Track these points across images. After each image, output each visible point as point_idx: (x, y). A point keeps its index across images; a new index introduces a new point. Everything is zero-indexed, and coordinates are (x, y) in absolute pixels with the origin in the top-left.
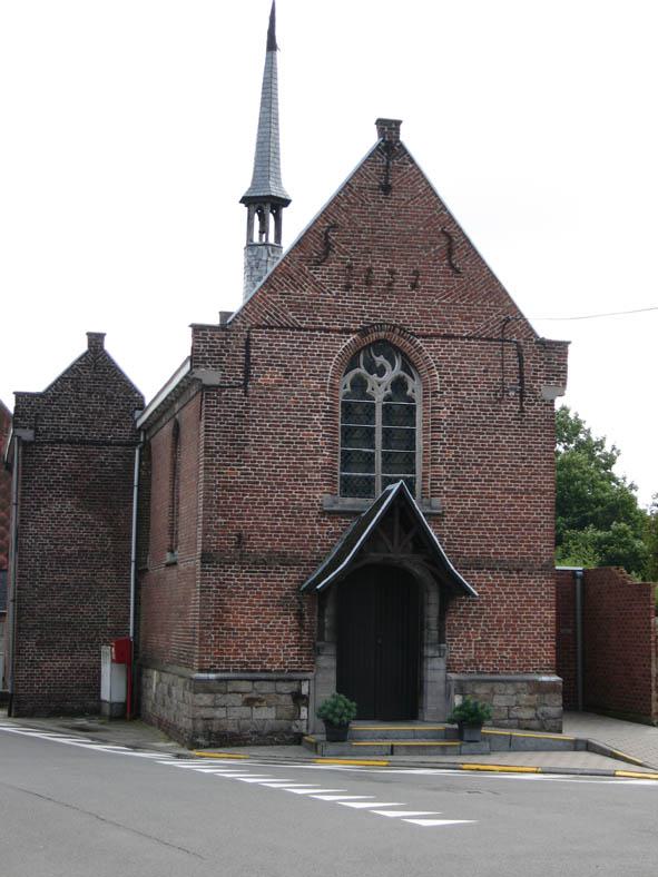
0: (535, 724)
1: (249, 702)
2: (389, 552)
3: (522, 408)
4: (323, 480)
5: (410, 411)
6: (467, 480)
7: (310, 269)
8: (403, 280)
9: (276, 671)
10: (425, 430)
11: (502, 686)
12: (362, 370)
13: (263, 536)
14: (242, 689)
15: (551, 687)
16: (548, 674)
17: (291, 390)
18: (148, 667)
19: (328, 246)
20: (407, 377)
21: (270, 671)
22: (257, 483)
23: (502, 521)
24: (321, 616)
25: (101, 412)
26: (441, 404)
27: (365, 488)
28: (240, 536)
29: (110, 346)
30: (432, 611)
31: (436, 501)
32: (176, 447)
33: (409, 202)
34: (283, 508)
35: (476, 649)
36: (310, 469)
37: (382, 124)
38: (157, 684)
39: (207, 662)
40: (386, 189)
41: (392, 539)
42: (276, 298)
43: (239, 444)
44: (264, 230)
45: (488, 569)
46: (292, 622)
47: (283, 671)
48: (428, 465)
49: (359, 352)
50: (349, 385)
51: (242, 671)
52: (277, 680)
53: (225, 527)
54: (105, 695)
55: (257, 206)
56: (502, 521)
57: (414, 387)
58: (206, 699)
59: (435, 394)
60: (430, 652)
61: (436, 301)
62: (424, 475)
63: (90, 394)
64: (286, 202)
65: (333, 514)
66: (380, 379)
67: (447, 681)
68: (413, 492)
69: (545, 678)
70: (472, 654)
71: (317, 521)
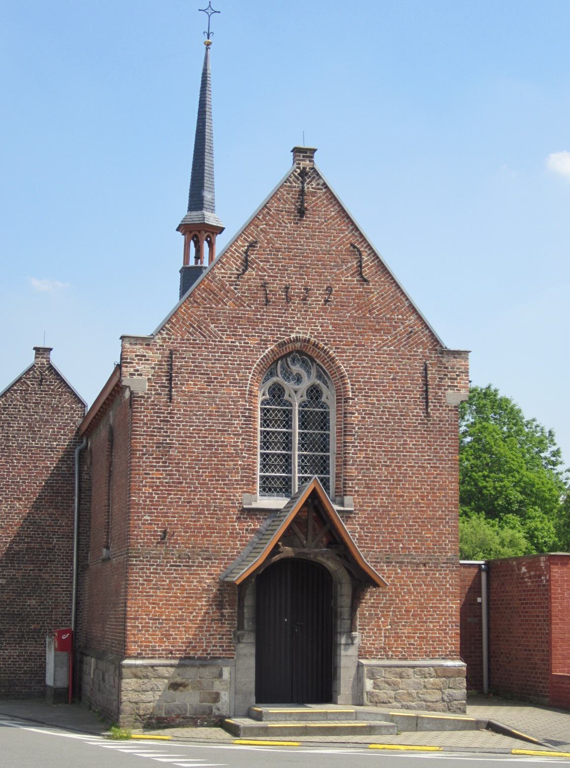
2: (304, 547)
6: (377, 480)
7: (231, 285)
9: (199, 658)
13: (187, 532)
15: (457, 672)
16: (453, 659)
18: (87, 655)
22: (181, 483)
24: (241, 607)
25: (47, 421)
30: (345, 600)
32: (111, 452)
33: (322, 223)
34: (205, 506)
35: (385, 637)
40: (302, 212)
44: (198, 256)
45: (397, 562)
46: (214, 613)
49: (276, 362)
51: (167, 658)
54: (50, 681)
57: (328, 396)
63: (37, 404)
66: (296, 387)
67: (360, 666)
68: (327, 488)
69: (449, 663)
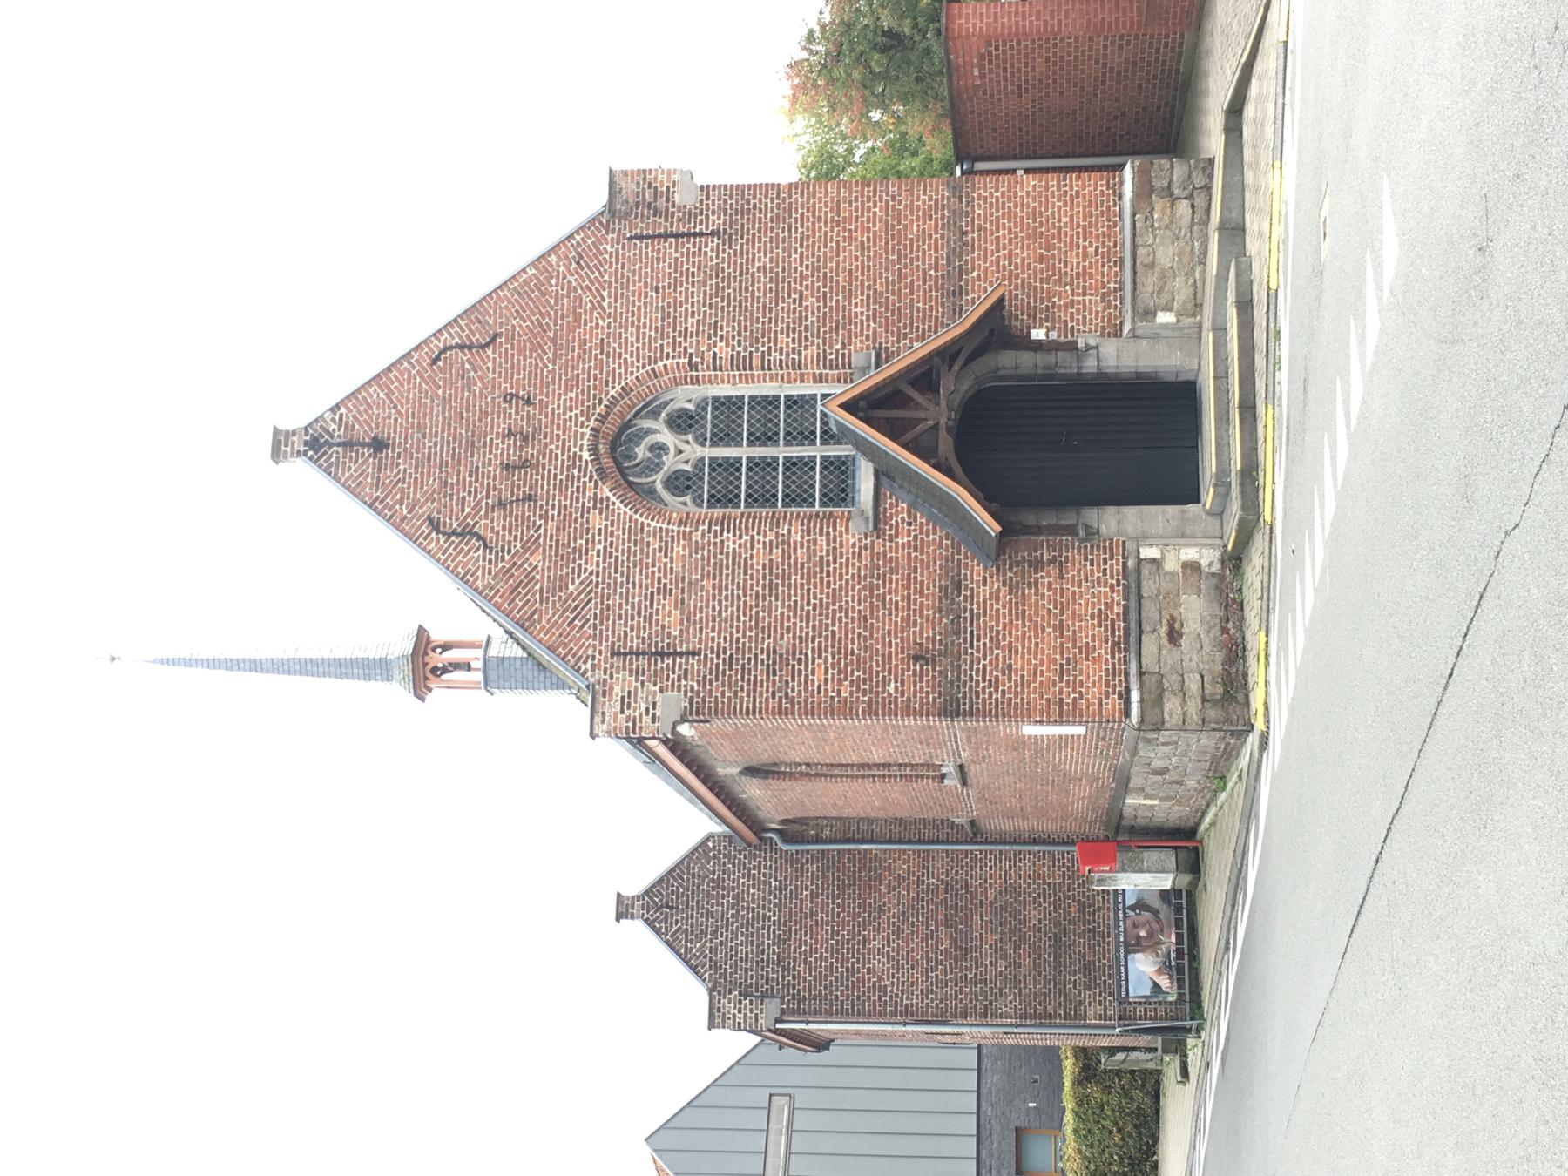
0: (1200, 201)
1: (1174, 636)
3: (712, 234)
4: (828, 533)
5: (726, 405)
7: (503, 560)
8: (515, 416)
10: (749, 379)
11: (1141, 251)
12: (658, 479)
13: (915, 622)
14: (1155, 650)
15: (1143, 178)
16: (1122, 183)
17: (690, 583)
19: (467, 532)
20: (668, 409)
21: (1126, 608)
22: (833, 632)
23: (887, 259)
25: (736, 897)
26: (708, 357)
27: (840, 471)
28: (916, 658)
29: (635, 886)
31: (857, 360)
35: (1084, 294)
36: (811, 553)
37: (277, 454)
38: (1147, 796)
39: (1113, 706)
40: (379, 445)
41: (918, 406)
42: (548, 613)
43: (774, 663)
46: (1048, 573)
47: (1126, 587)
48: (802, 375)
49: (630, 484)
50: (682, 499)
52: (1140, 597)
53: (903, 682)
55: (429, 675)
56: (887, 259)
57: (684, 397)
58: (1171, 705)
59: (693, 366)
60: (1090, 365)
61: (551, 366)
62: (819, 379)
63: (709, 914)
64: (422, 635)
65: (878, 520)
70: (1093, 300)
71: (891, 541)
